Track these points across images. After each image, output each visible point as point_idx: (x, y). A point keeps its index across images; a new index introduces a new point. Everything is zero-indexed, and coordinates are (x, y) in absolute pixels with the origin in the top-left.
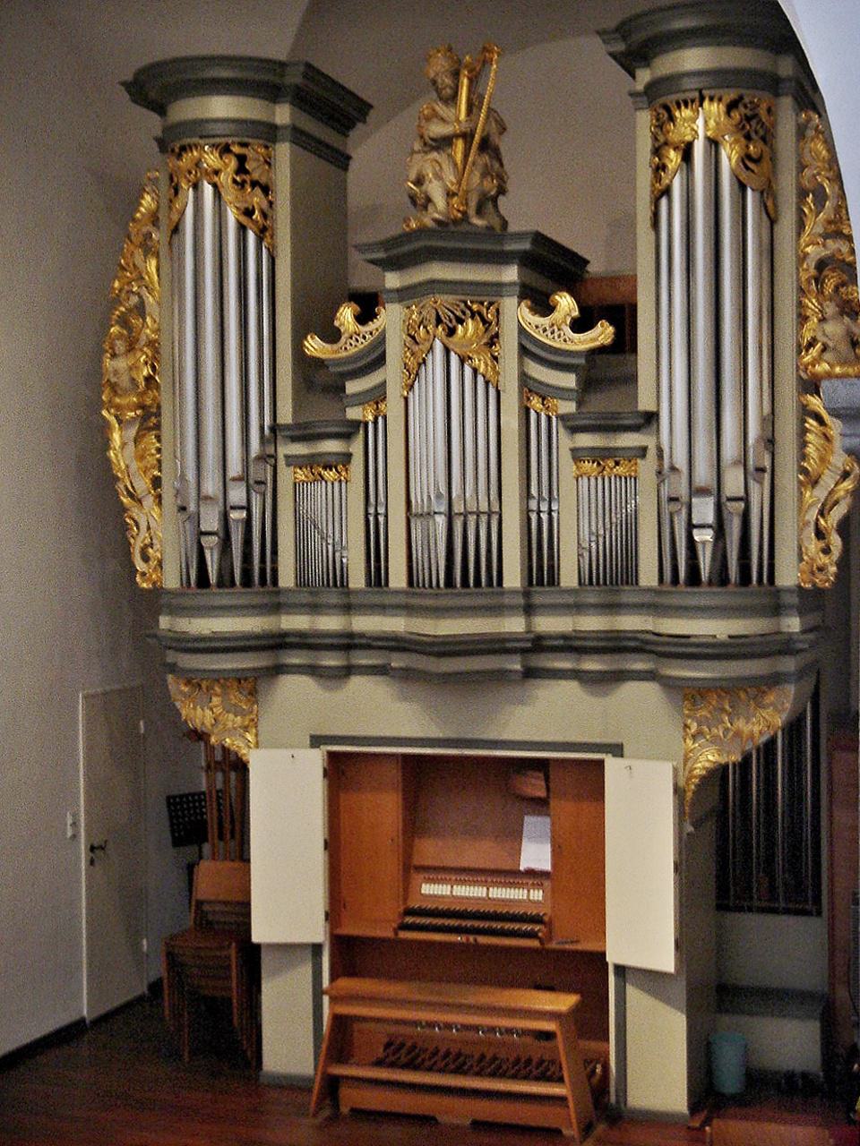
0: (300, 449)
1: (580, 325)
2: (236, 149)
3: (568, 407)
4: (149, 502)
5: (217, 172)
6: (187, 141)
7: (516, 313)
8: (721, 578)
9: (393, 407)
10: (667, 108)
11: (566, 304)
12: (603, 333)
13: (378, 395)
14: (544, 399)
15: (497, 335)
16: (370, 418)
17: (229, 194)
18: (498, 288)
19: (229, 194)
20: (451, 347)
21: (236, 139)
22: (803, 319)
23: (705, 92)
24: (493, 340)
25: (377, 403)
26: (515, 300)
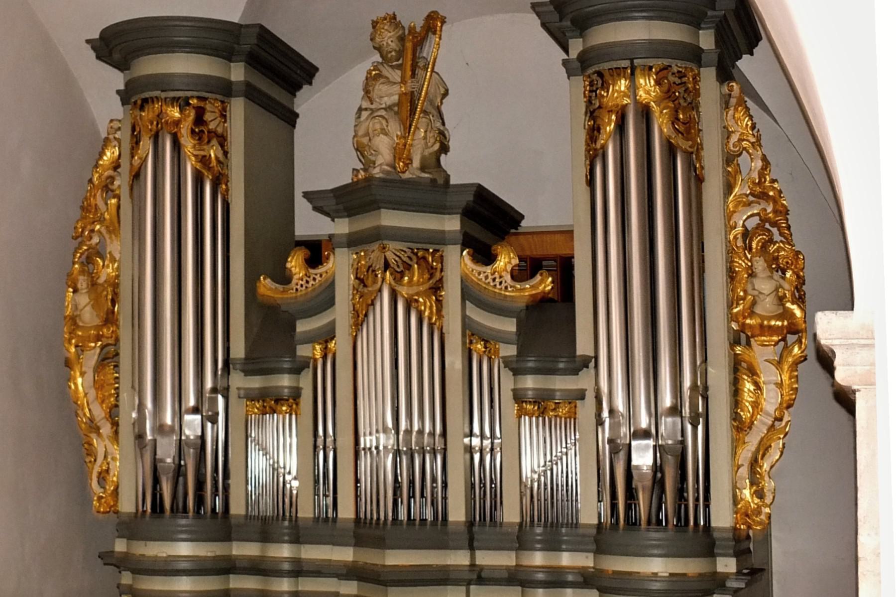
0: (256, 383)
1: (521, 274)
2: (194, 102)
3: (509, 351)
4: (106, 429)
5: (177, 123)
6: (146, 95)
7: (458, 263)
8: (649, 522)
9: (341, 345)
10: (600, 74)
11: (505, 261)
12: (545, 284)
13: (327, 335)
14: (486, 341)
15: (441, 280)
16: (318, 354)
17: (188, 144)
18: (440, 239)
19: (188, 144)
20: (398, 288)
21: (195, 94)
22: (731, 274)
23: (636, 62)
24: (436, 288)
25: (327, 342)
26: (458, 247)
